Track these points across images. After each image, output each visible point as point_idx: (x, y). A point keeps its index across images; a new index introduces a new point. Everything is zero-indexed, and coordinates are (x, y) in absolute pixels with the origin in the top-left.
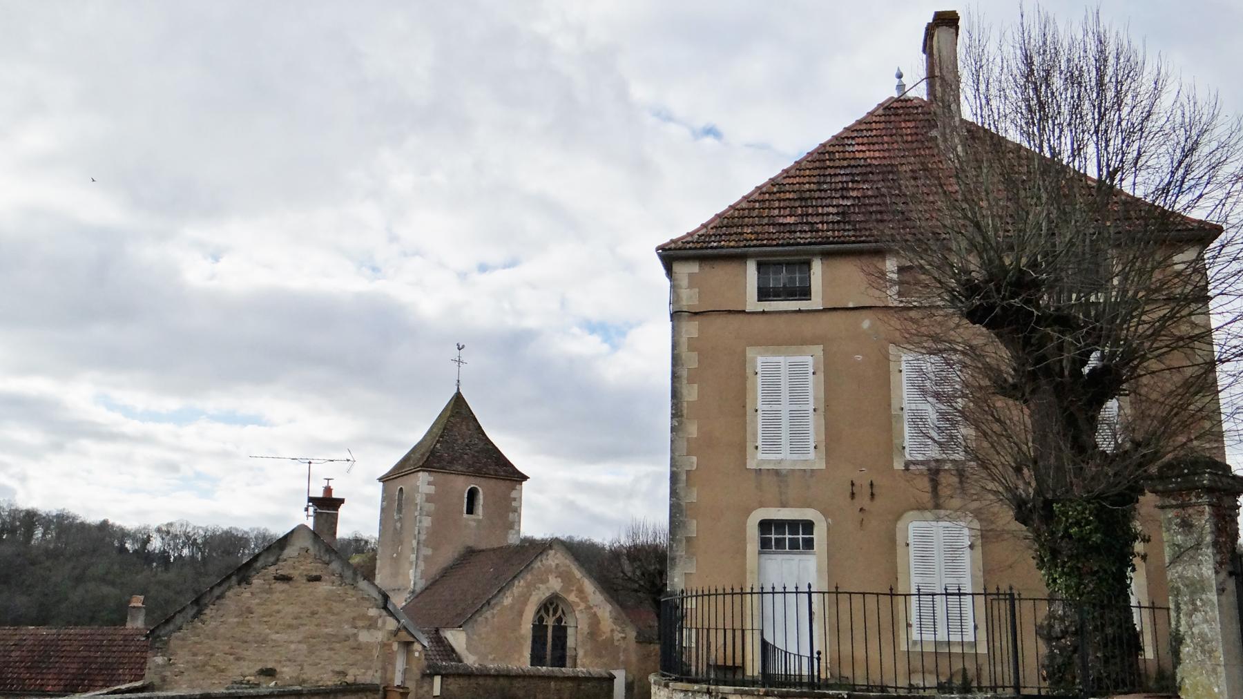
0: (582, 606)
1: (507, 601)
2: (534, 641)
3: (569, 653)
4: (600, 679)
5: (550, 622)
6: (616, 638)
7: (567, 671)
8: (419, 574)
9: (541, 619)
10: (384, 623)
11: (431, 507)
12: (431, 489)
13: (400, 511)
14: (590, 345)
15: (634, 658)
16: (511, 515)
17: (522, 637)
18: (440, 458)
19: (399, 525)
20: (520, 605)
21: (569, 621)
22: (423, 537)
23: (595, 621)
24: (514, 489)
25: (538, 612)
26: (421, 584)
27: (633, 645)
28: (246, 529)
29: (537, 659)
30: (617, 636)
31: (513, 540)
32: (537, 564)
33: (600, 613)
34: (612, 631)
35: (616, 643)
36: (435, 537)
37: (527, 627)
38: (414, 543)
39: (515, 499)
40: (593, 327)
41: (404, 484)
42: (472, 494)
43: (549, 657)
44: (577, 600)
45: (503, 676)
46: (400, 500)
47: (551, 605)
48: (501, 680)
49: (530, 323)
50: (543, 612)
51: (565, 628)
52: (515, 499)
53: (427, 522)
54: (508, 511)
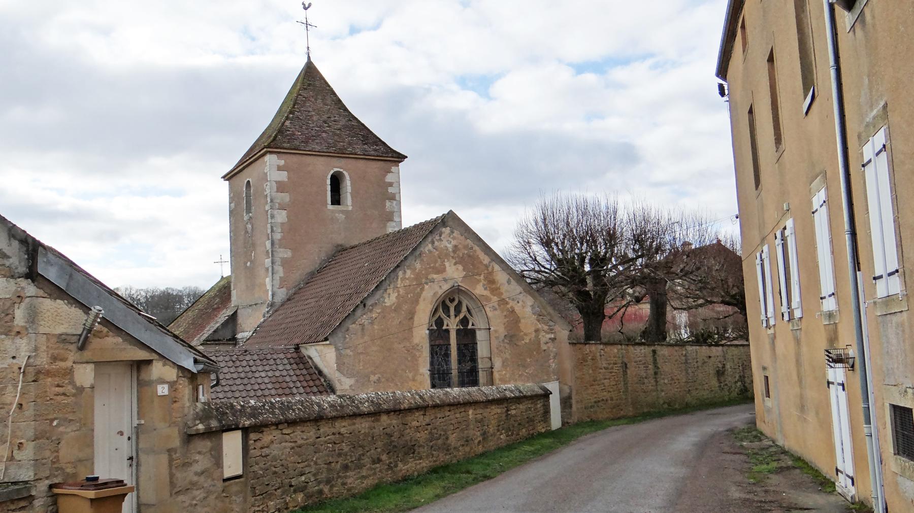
0: (495, 299)
1: (390, 298)
3: (482, 365)
4: (534, 398)
5: (452, 324)
6: (543, 340)
7: (483, 391)
8: (277, 282)
9: (439, 322)
10: (33, 317)
11: (286, 197)
12: (283, 176)
13: (249, 210)
14: (464, 101)
15: (568, 365)
16: (388, 204)
17: (415, 347)
18: (292, 138)
20: (409, 308)
21: (477, 322)
22: (278, 236)
23: (513, 320)
25: (436, 310)
26: (282, 294)
27: (566, 348)
28: (180, 288)
29: (440, 377)
30: (545, 337)
31: (391, 228)
32: (428, 247)
33: (518, 308)
34: (537, 331)
35: (544, 347)
36: (293, 234)
37: (421, 334)
38: (268, 244)
39: (391, 184)
40: (464, 82)
41: (249, 175)
42: (336, 181)
44: (487, 293)
45: (388, 412)
46: (248, 196)
47: (450, 301)
48: (384, 418)
49: (407, 80)
50: (441, 312)
51: (473, 332)
52: (391, 184)
53: (281, 216)
54: (385, 198)
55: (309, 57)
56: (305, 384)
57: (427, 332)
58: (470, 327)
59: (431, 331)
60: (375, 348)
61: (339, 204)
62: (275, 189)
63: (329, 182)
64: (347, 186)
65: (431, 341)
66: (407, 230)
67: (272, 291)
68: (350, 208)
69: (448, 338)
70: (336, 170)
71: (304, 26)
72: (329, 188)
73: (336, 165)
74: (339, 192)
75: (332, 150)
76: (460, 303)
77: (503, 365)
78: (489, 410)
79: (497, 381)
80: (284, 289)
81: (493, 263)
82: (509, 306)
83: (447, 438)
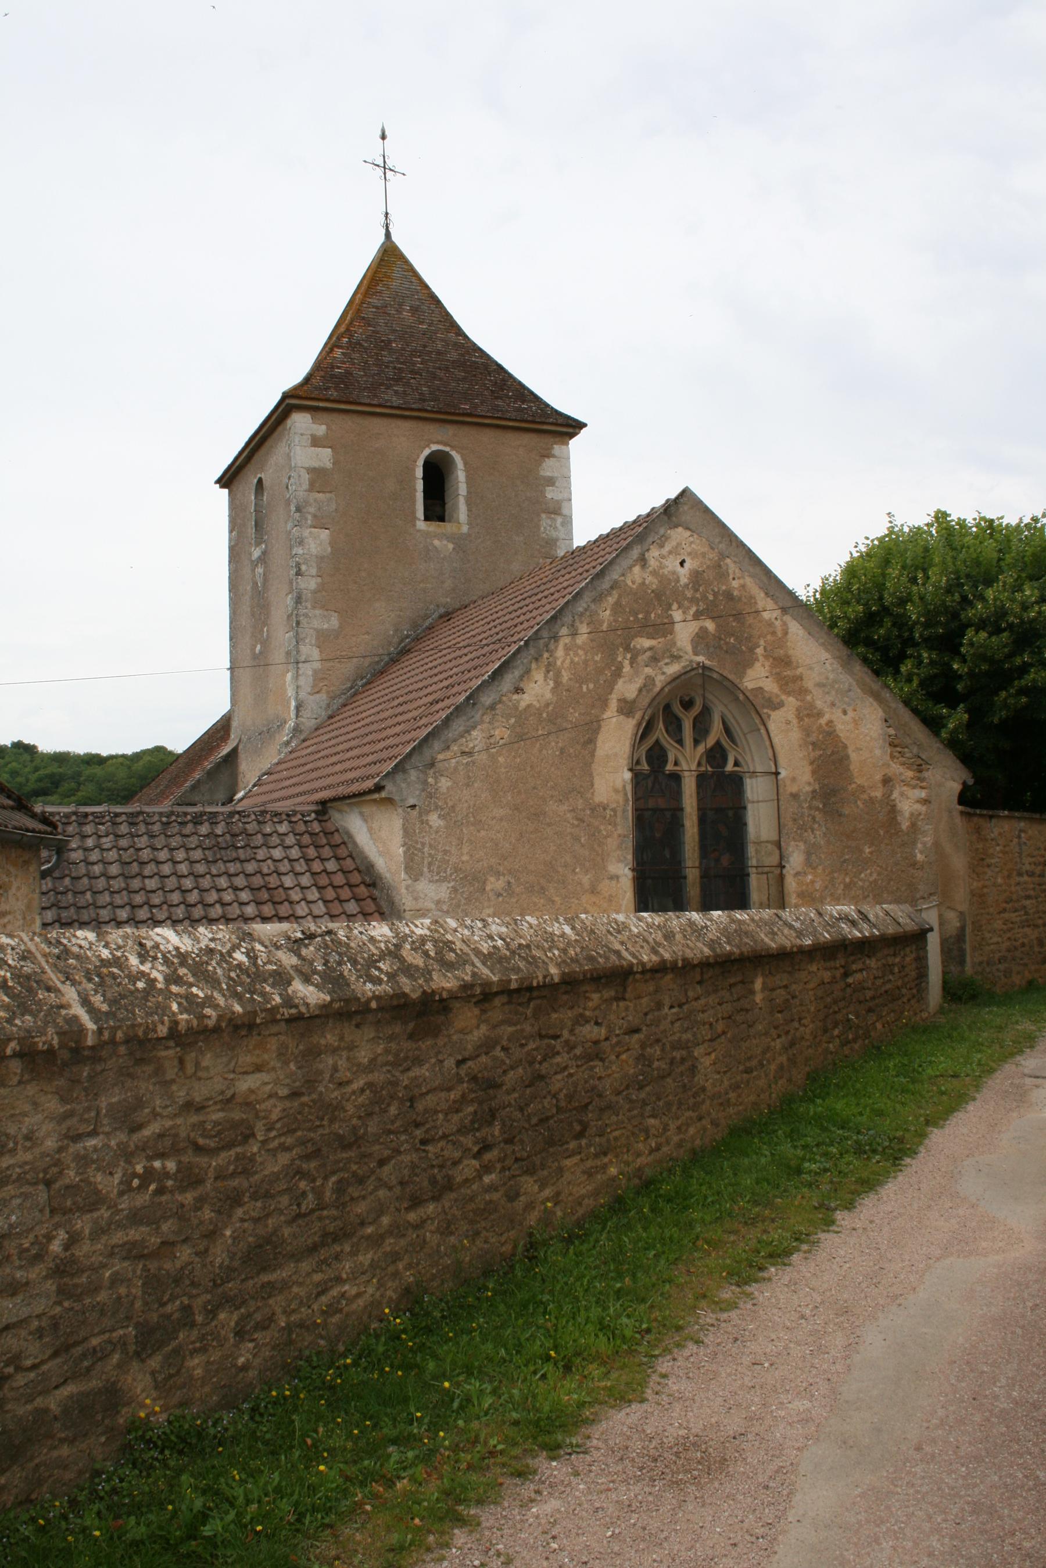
2: (642, 820)
3: (757, 855)
5: (687, 761)
7: (755, 924)
8: (306, 681)
9: (657, 756)
12: (324, 457)
19: (260, 570)
21: (751, 758)
22: (309, 584)
24: (549, 456)
26: (316, 706)
29: (657, 888)
33: (843, 727)
37: (613, 775)
42: (437, 475)
43: (692, 873)
50: (660, 732)
51: (736, 782)
52: (551, 482)
53: (317, 542)
54: (540, 502)
55: (388, 235)
56: (330, 894)
57: (628, 775)
58: (729, 767)
59: (638, 778)
60: (499, 812)
61: (442, 519)
62: (306, 486)
63: (419, 473)
64: (460, 478)
65: (636, 799)
66: (582, 549)
67: (296, 699)
68: (465, 529)
69: (678, 794)
70: (435, 447)
71: (380, 171)
72: (420, 485)
73: (433, 441)
74: (443, 504)
75: (430, 405)
76: (706, 711)
77: (808, 863)
78: (803, 975)
79: (793, 899)
80: (323, 696)
81: (787, 618)
82: (823, 721)
83: (693, 1070)
